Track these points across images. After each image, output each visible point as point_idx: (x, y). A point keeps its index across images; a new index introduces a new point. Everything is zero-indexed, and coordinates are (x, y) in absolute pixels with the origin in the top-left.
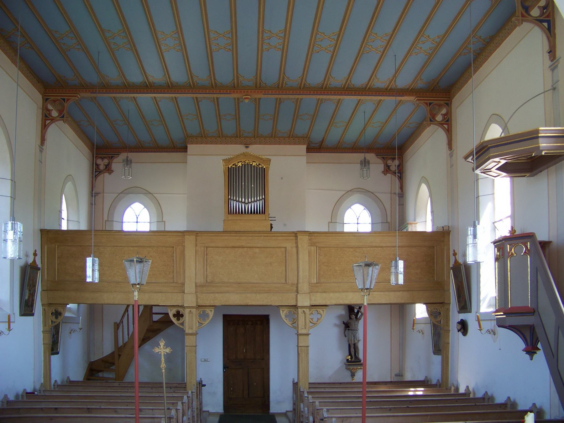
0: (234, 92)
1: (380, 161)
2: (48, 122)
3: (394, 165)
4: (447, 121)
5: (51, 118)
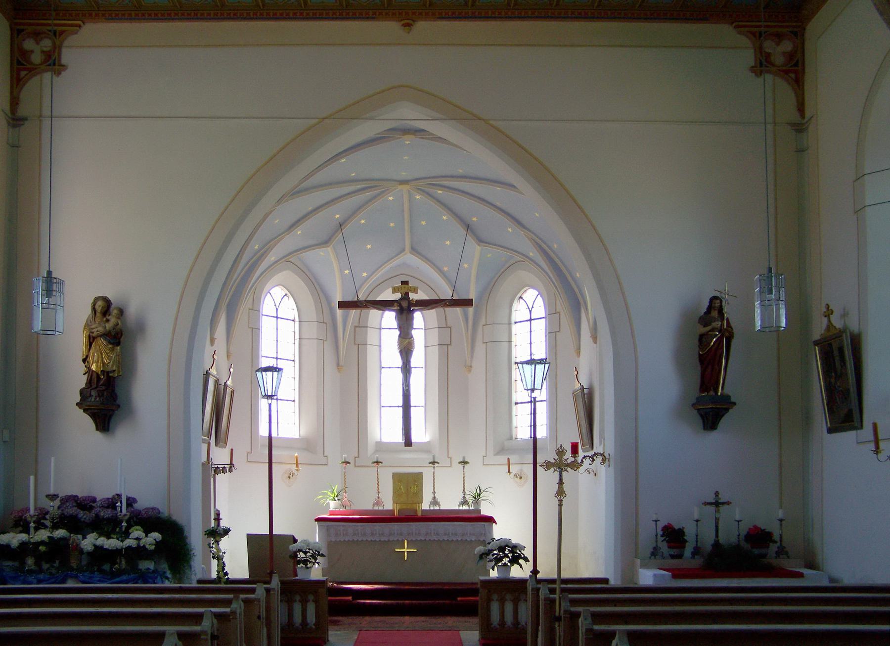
0: (380, 14)
1: (744, 41)
2: (23, 73)
3: (779, 51)
4: (796, 65)
5: (29, 66)
